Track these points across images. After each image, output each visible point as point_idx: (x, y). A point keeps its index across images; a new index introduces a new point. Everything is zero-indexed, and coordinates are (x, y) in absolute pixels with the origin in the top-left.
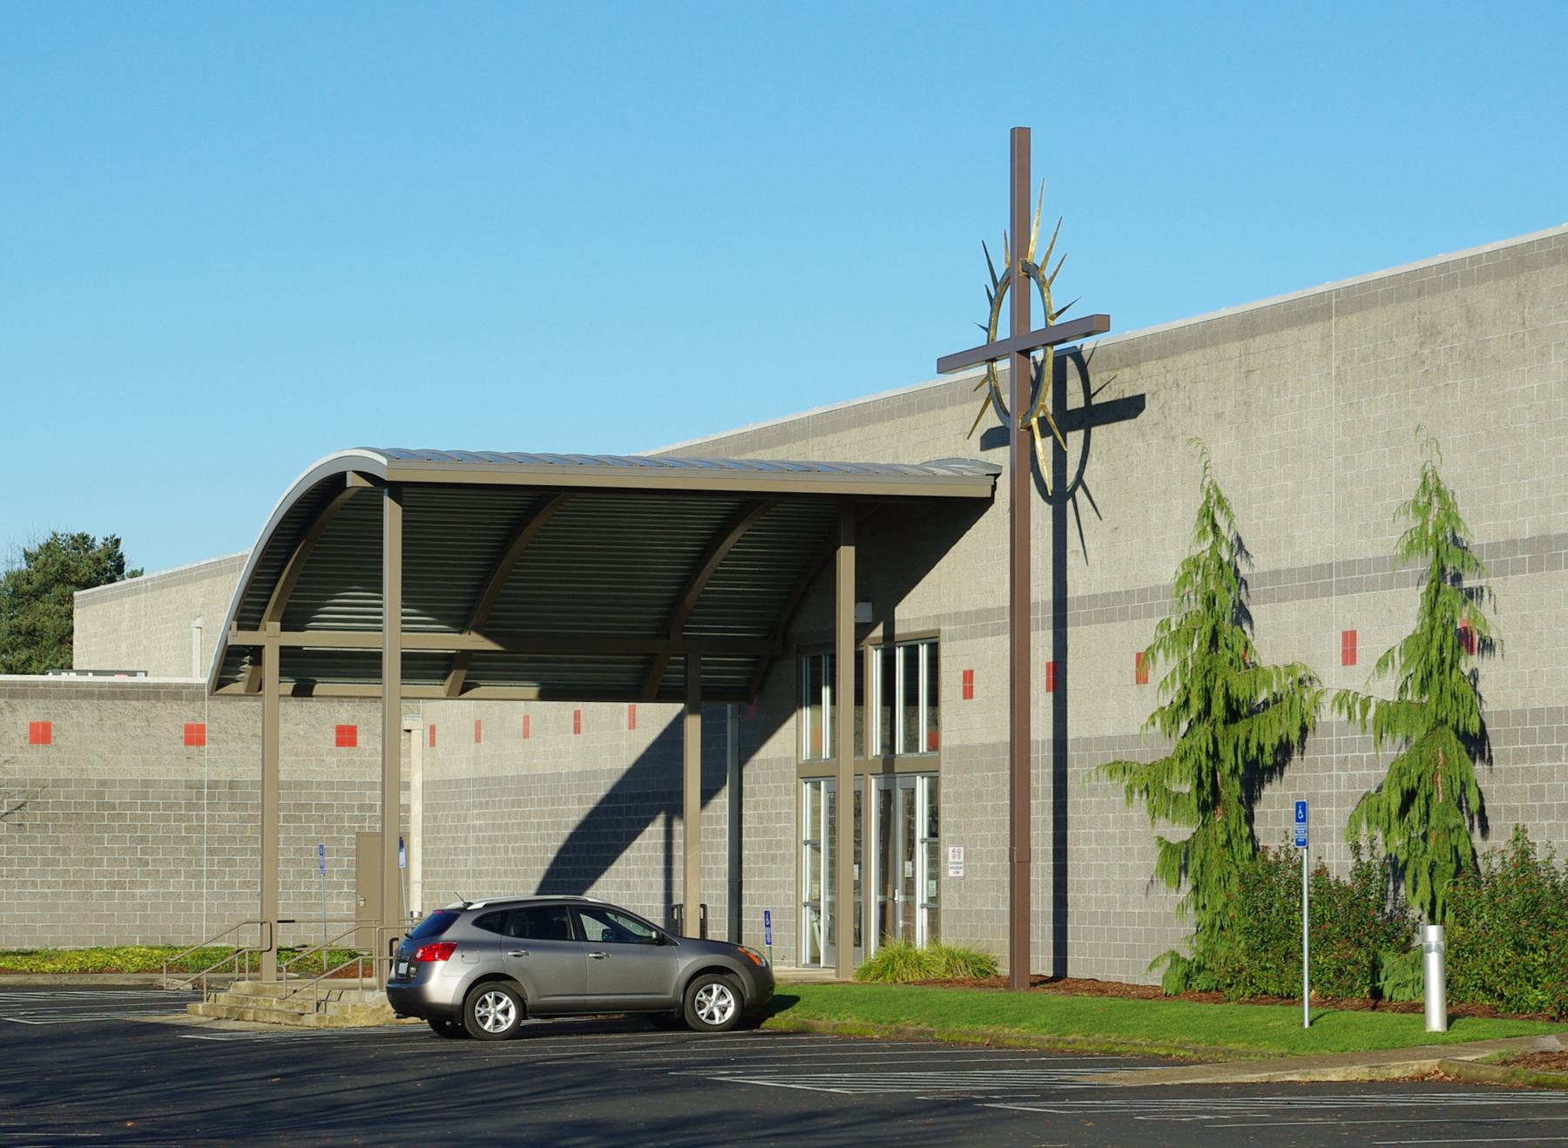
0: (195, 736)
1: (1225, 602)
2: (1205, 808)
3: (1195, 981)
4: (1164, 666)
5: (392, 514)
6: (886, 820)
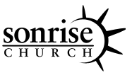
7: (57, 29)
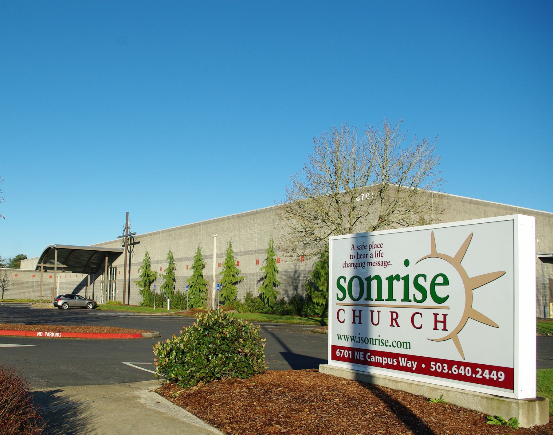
0: (34, 276)
1: (148, 264)
2: (145, 286)
3: (143, 305)
4: (141, 271)
5: (56, 251)
6: (110, 287)
7: (398, 278)
